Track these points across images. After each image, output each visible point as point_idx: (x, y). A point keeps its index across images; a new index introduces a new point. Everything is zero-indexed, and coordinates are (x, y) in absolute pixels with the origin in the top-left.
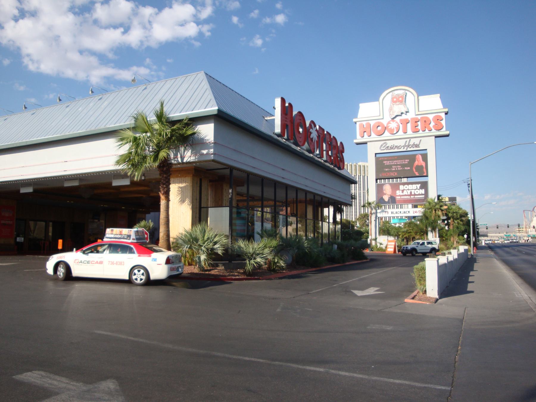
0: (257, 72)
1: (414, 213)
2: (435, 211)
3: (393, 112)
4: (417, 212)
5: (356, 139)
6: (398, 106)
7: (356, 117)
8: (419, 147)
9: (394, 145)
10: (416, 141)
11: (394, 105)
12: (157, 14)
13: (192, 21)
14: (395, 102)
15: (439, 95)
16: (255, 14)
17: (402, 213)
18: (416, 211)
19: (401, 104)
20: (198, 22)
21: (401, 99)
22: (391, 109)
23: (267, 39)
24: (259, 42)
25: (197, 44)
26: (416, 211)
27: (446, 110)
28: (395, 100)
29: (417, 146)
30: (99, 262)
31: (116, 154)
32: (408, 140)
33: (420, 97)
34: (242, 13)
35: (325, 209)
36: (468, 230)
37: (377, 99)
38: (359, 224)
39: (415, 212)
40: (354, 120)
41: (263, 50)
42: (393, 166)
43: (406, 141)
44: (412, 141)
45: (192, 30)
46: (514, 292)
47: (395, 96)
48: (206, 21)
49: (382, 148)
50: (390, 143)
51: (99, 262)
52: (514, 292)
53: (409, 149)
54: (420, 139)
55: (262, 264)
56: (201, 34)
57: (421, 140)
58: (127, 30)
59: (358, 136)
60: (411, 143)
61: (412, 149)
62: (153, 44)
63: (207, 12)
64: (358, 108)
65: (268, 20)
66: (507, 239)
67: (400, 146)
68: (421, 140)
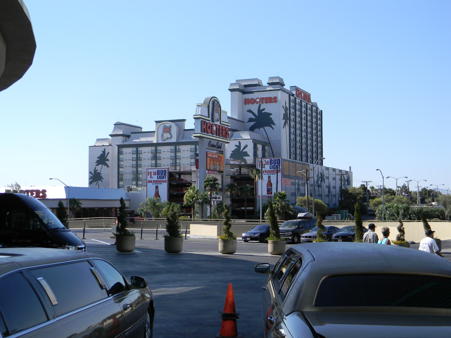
3: (163, 137)
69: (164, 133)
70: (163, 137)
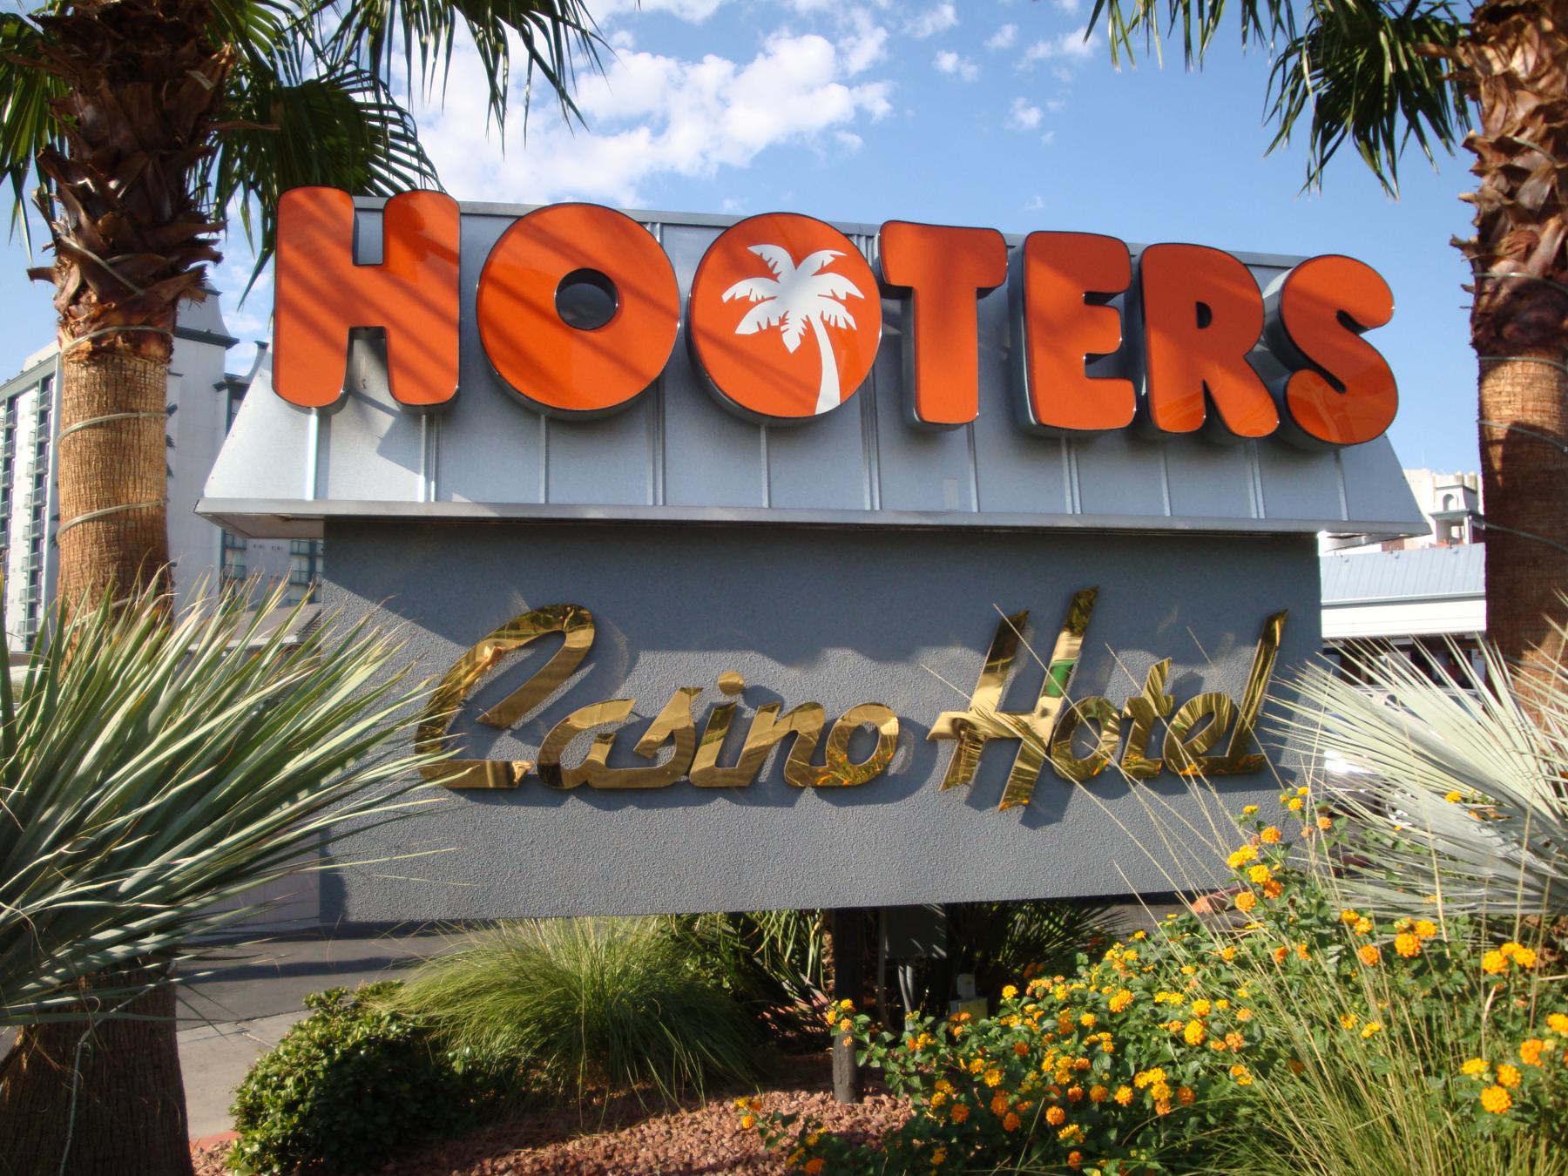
0: (1040, 204)
12: (737, 74)
13: (832, 82)
16: (1006, 36)
20: (849, 81)
23: (1052, 105)
24: (1032, 117)
25: (854, 141)
30: (1485, 422)
31: (1443, 148)
34: (964, 39)
35: (1327, 632)
36: (1383, 971)
38: (1252, 812)
41: (1048, 138)
45: (835, 103)
48: (872, 74)
51: (1485, 422)
56: (862, 113)
58: (659, 125)
62: (739, 160)
63: (869, 48)
65: (1042, 50)
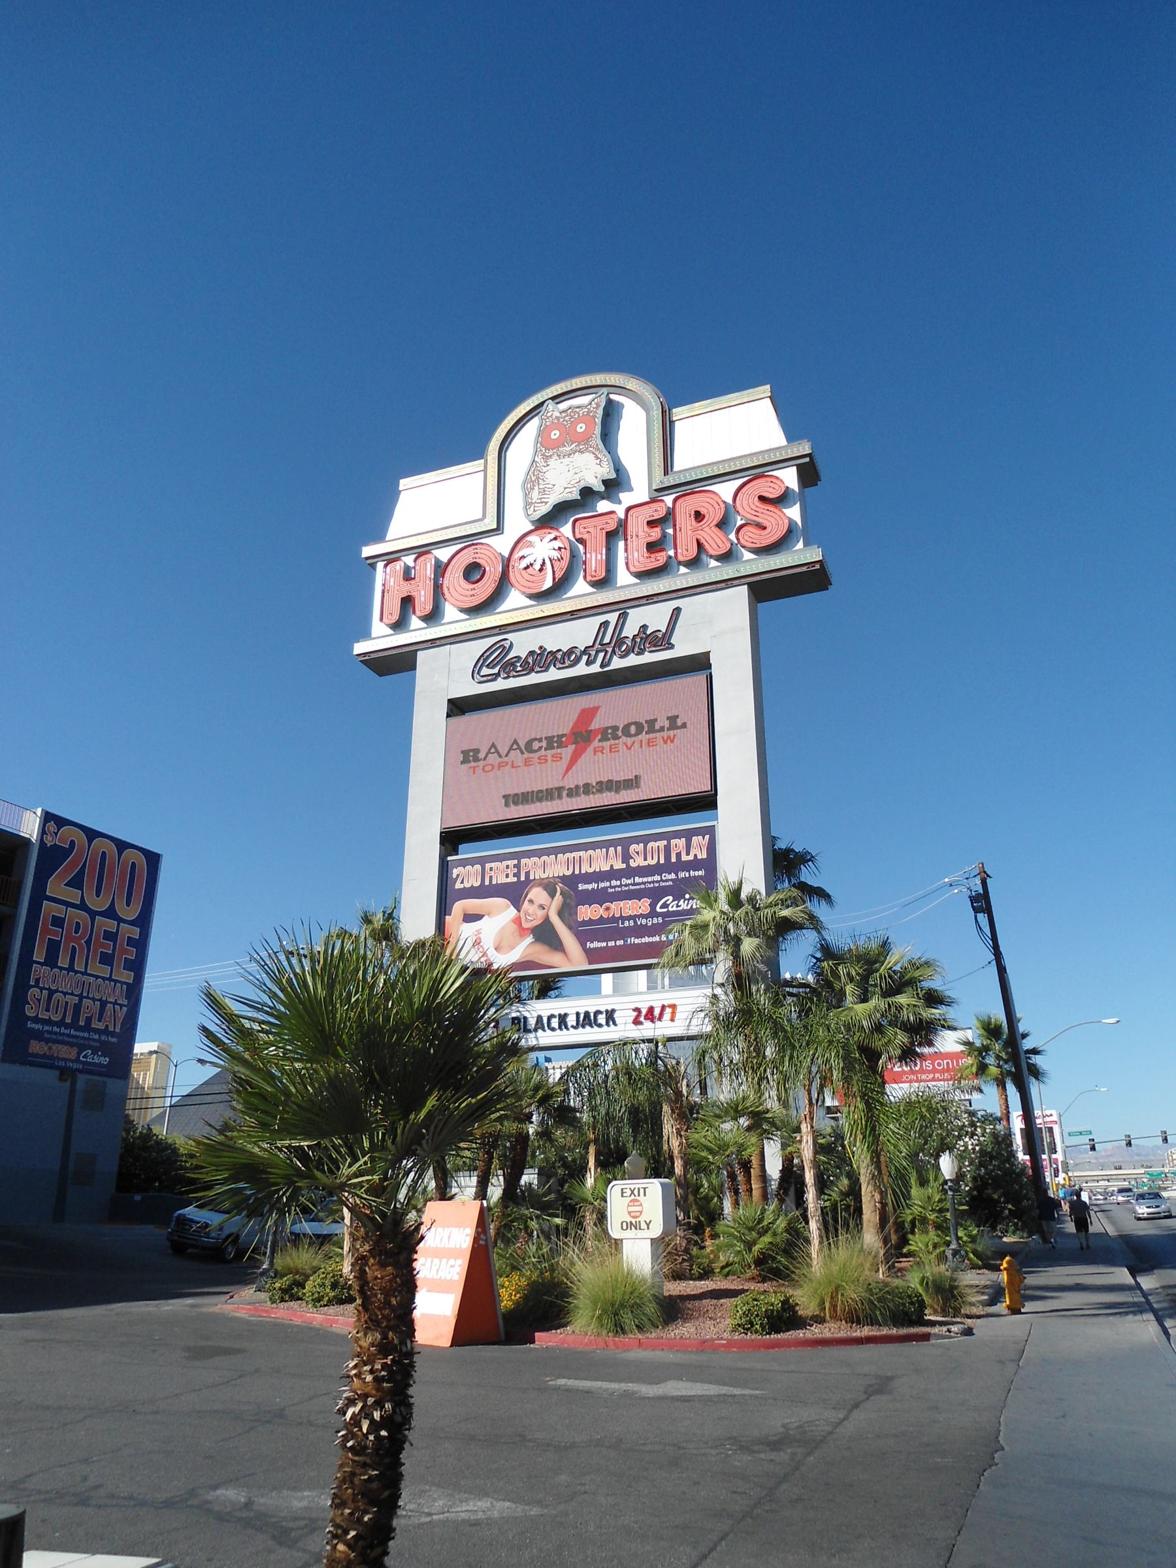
1: (636, 1022)
2: (759, 909)
3: (543, 492)
4: (657, 1012)
5: (366, 634)
6: (567, 460)
7: (379, 535)
8: (671, 647)
9: (541, 648)
10: (655, 617)
11: (552, 462)
14: (557, 444)
15: (766, 390)
17: (570, 1024)
18: (651, 1009)
19: (581, 452)
21: (581, 428)
22: (533, 478)
26: (651, 1009)
27: (805, 448)
28: (555, 435)
29: (662, 640)
32: (613, 618)
33: (678, 413)
37: (478, 453)
39: (644, 1012)
40: (368, 551)
42: (580, 885)
43: (605, 624)
44: (636, 619)
46: (284, 982)
47: (557, 418)
49: (485, 671)
50: (523, 644)
52: (284, 982)
53: (617, 663)
54: (668, 607)
55: (1140, 1204)
57: (677, 611)
59: (379, 628)
60: (630, 630)
61: (633, 660)
64: (394, 495)
66: (359, 1301)
67: (571, 651)
68: (677, 611)
69: (546, 458)
70: (535, 495)
